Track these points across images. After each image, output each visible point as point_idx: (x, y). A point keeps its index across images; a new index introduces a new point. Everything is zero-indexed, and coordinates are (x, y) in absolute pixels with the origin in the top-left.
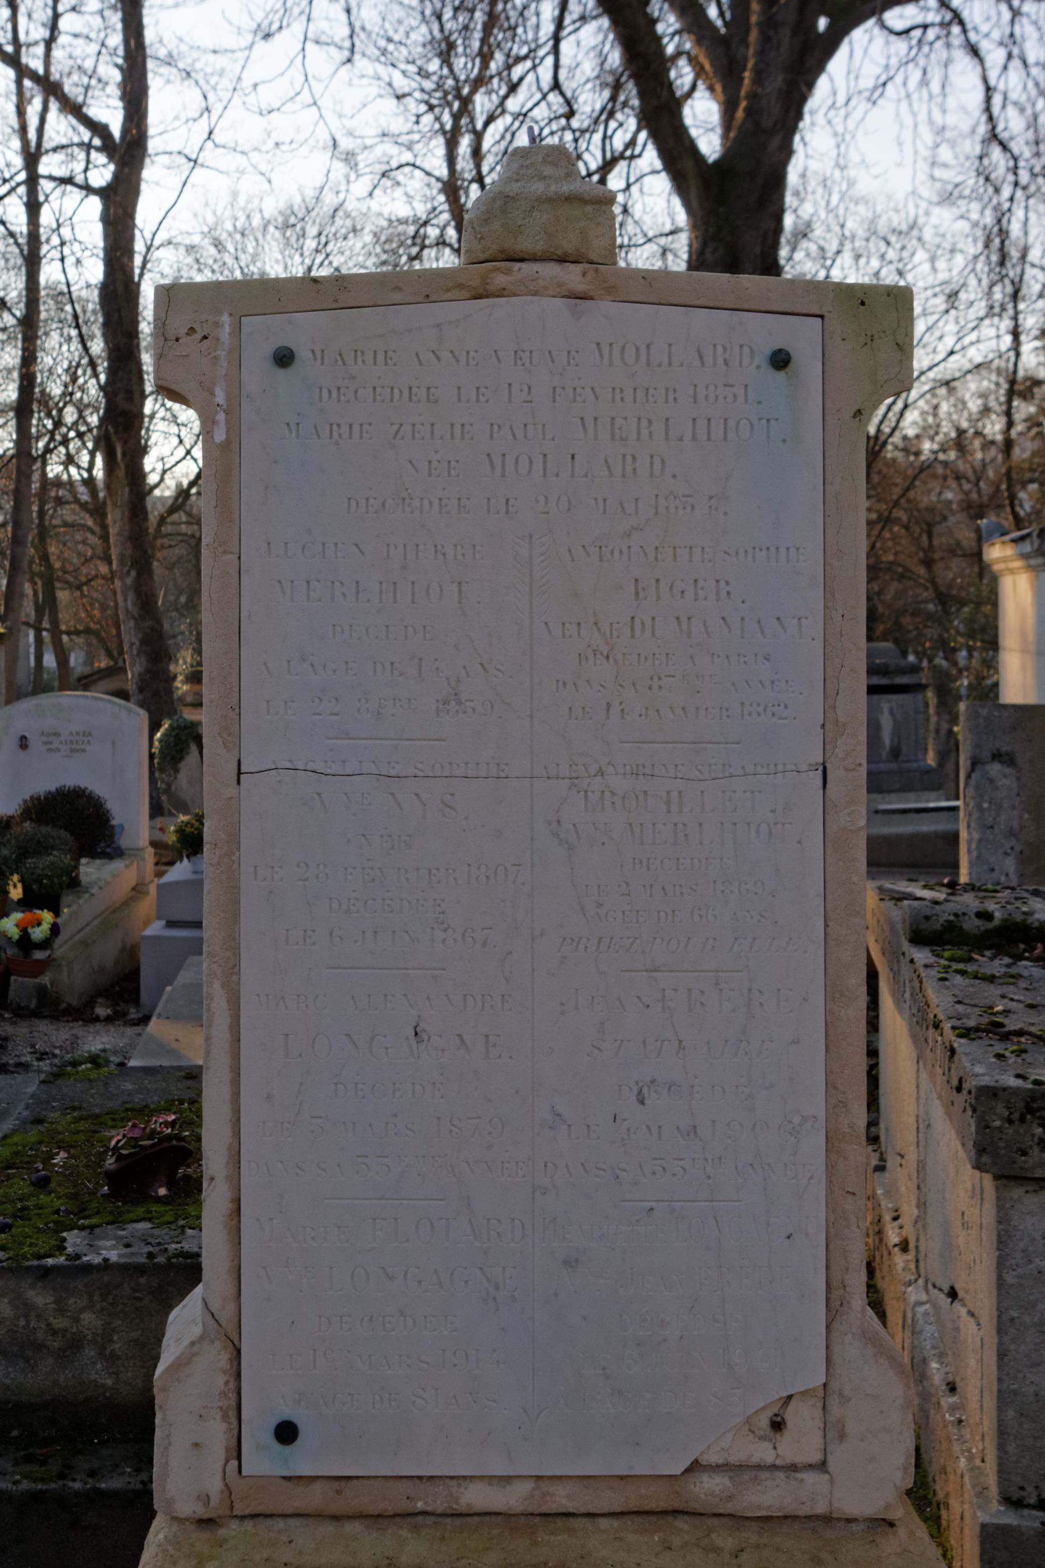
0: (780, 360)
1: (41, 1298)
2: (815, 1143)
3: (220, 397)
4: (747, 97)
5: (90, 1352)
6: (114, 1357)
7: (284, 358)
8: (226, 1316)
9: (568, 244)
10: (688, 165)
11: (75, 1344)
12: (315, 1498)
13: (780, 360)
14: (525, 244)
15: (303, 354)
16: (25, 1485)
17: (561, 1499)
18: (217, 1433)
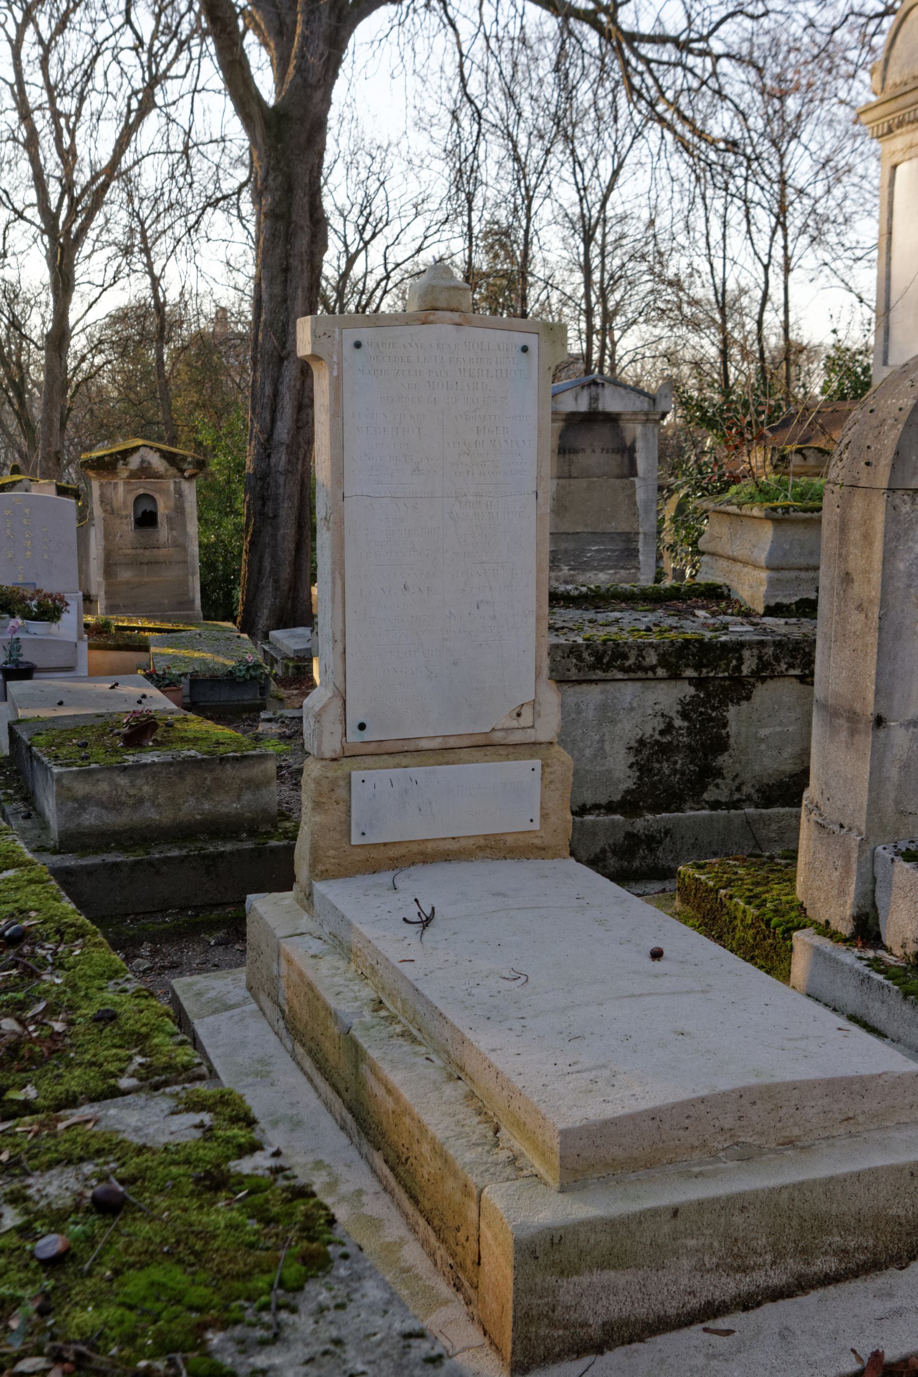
0: (525, 349)
1: (123, 780)
2: (532, 620)
3: (335, 359)
4: (296, 57)
5: (148, 804)
6: (159, 805)
7: (358, 345)
8: (341, 688)
9: (454, 305)
10: (255, 110)
11: (140, 801)
12: (371, 748)
13: (525, 349)
14: (440, 304)
15: (364, 343)
16: (132, 858)
17: (452, 743)
18: (339, 729)
